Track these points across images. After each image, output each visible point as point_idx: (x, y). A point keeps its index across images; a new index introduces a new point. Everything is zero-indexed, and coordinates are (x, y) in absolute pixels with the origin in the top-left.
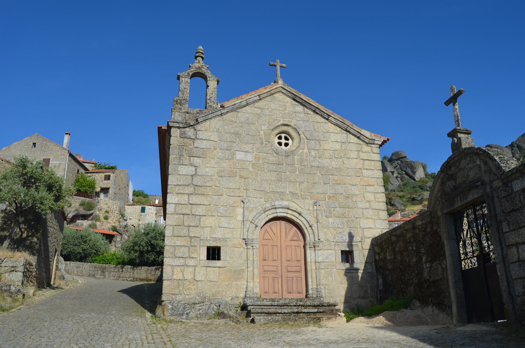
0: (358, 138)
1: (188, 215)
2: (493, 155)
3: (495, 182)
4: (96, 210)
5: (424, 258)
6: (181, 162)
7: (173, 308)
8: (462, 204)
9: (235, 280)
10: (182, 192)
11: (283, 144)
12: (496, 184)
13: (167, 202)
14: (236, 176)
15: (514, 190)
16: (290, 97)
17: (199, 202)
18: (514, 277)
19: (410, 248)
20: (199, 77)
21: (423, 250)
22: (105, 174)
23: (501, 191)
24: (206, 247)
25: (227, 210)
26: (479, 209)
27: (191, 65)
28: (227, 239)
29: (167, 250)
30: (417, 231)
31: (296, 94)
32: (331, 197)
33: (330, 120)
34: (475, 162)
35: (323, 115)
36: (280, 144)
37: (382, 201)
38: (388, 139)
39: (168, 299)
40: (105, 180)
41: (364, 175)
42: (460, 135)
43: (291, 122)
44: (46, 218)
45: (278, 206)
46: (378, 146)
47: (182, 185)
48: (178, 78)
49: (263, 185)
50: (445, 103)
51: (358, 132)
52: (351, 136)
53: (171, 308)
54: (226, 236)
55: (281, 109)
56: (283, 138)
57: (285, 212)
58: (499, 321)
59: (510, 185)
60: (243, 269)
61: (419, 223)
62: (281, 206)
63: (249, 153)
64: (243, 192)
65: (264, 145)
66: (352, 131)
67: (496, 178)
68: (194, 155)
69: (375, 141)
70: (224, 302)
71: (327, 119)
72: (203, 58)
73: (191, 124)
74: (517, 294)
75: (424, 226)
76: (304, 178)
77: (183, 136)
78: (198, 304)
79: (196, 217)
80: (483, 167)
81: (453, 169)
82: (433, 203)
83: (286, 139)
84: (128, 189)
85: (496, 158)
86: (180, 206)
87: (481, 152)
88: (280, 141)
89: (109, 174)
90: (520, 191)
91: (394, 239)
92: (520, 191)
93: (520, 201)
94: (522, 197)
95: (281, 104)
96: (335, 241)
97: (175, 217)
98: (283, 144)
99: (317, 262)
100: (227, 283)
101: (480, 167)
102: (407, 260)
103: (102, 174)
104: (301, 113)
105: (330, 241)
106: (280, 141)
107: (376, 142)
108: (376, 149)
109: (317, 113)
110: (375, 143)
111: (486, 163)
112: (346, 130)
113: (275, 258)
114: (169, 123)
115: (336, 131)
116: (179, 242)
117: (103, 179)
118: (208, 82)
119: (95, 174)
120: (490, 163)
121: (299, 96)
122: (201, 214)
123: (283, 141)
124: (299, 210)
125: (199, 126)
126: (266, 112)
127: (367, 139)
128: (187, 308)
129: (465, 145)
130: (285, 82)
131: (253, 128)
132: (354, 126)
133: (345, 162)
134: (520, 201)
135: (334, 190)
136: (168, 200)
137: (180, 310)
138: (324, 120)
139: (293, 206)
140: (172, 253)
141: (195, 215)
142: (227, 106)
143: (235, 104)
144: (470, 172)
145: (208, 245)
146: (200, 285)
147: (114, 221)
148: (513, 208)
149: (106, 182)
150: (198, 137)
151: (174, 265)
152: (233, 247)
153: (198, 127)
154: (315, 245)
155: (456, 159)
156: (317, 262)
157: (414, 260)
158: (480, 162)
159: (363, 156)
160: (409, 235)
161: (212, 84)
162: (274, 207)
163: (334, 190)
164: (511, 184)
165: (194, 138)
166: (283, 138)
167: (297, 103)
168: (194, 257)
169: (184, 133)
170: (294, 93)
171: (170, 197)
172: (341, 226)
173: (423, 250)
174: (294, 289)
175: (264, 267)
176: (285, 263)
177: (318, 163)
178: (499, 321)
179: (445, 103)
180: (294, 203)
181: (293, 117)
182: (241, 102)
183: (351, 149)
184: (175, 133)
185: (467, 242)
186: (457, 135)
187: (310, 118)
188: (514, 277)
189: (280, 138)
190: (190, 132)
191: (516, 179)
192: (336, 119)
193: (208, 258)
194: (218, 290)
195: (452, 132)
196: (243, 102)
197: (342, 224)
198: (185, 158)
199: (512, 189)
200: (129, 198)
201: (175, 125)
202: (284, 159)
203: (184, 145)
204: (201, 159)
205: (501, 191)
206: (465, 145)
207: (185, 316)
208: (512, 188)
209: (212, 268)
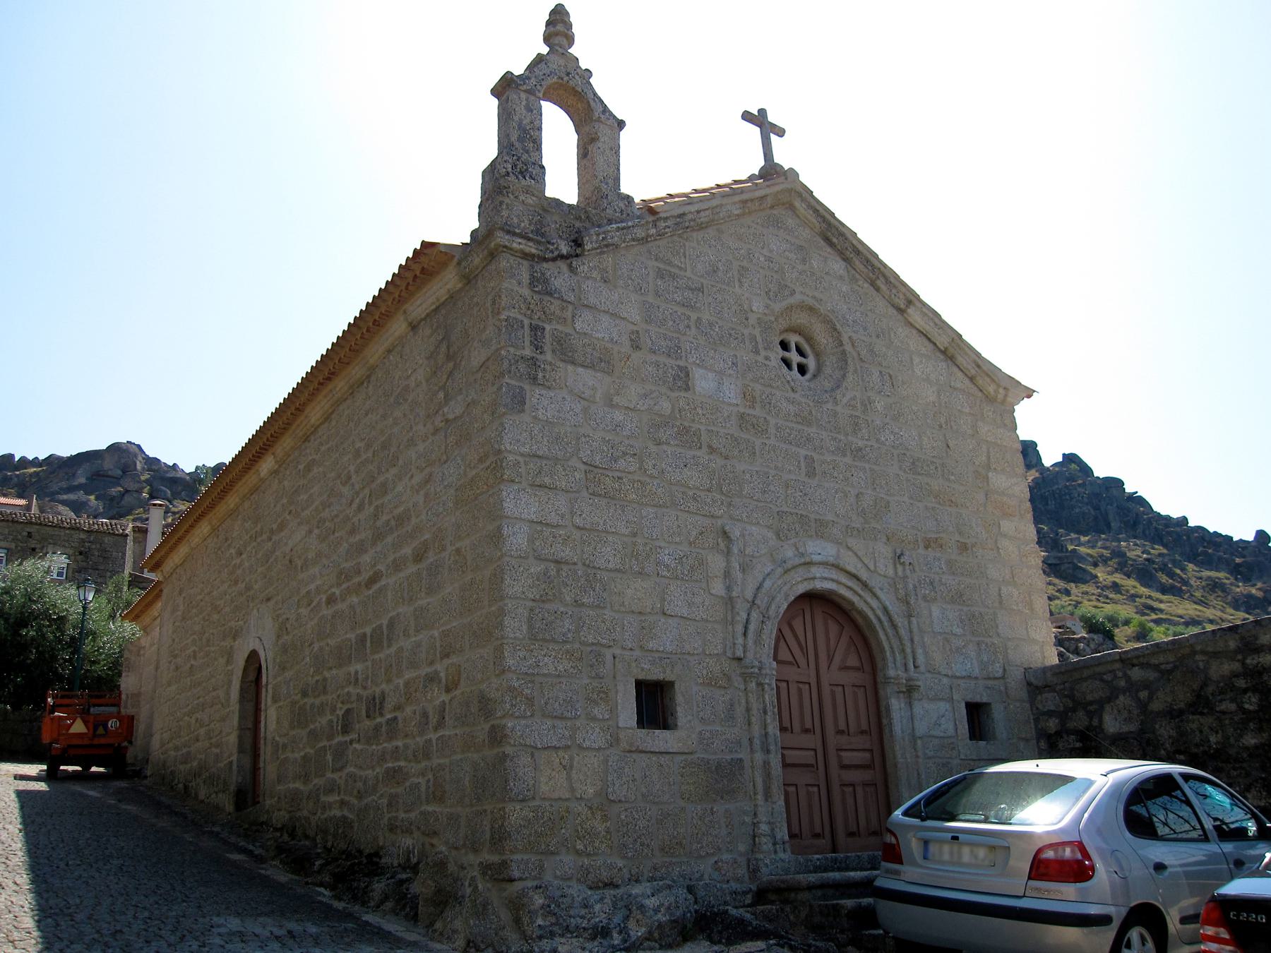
24: (985, 700)
25: (684, 559)
49: (772, 488)
53: (542, 907)
54: (688, 648)
58: (94, 769)
60: (741, 760)
64: (722, 504)
106: (787, 354)
113: (808, 725)
123: (795, 358)
133: (950, 445)
145: (640, 677)
151: (539, 746)
154: (911, 683)
174: (862, 822)
175: (843, 754)
176: (832, 740)
178: (94, 769)
182: (698, 212)
189: (784, 345)
193: (641, 723)
196: (702, 214)
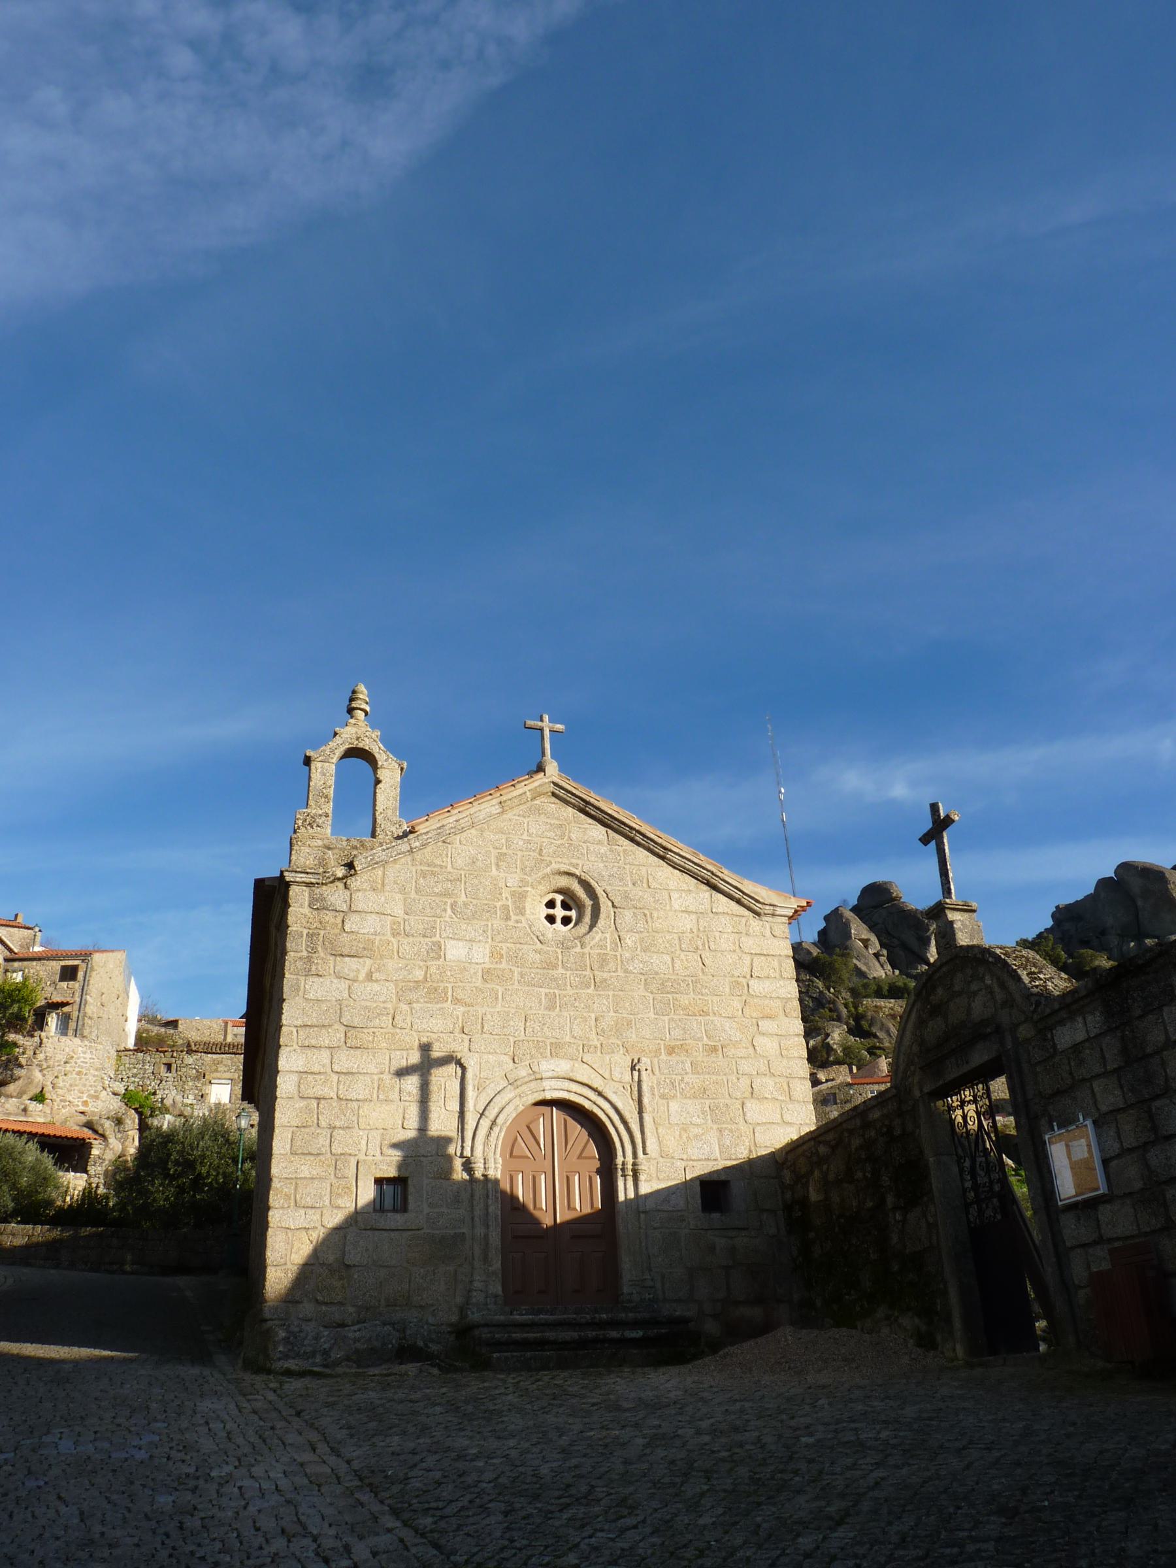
0: (739, 902)
1: (329, 1101)
2: (1015, 967)
3: (1021, 1028)
4: (34, 1067)
5: (890, 1200)
6: (314, 968)
7: (289, 1338)
8: (960, 1073)
9: (443, 1263)
10: (313, 1042)
11: (559, 920)
12: (1025, 1031)
13: (279, 1069)
14: (447, 1001)
15: (1058, 1047)
16: (574, 806)
17: (356, 1066)
18: (1068, 1244)
19: (859, 1175)
20: (357, 757)
21: (885, 1180)
22: (63, 963)
23: (1034, 1048)
26: (971, 1100)
27: (337, 729)
28: (422, 1159)
29: (278, 1189)
30: (873, 1133)
31: (588, 799)
32: (673, 1048)
33: (669, 860)
34: (982, 979)
35: (652, 847)
36: (551, 919)
37: (796, 1055)
38: (808, 903)
39: (276, 1316)
40: (62, 979)
41: (753, 993)
42: (951, 916)
43: (575, 866)
44: (856, 1328)
45: (547, 1073)
46: (785, 920)
47: (316, 1026)
48: (307, 761)
49: (511, 1023)
50: (920, 839)
51: (736, 888)
52: (720, 896)
53: (283, 1339)
55: (551, 834)
56: (558, 904)
57: (563, 1087)
59: (1049, 1036)
61: (876, 1115)
62: (555, 1074)
63: (479, 944)
64: (462, 1041)
65: (511, 923)
66: (722, 886)
67: (1023, 1019)
68: (345, 951)
69: (778, 909)
70: (415, 1320)
71: (663, 858)
72: (366, 713)
73: (338, 876)
74: (1076, 1282)
75: (887, 1122)
76: (609, 1003)
77: (320, 906)
78: (352, 1325)
79: (349, 1105)
80: (1000, 996)
81: (940, 991)
82: (902, 1068)
83: (565, 906)
84: (125, 1005)
85: (1023, 974)
86: (310, 1078)
87: (991, 959)
88: (551, 911)
89: (76, 963)
90: (1070, 1051)
91: (822, 1150)
92: (1070, 1051)
93: (1071, 1074)
94: (1073, 1064)
95: (552, 822)
96: (685, 1157)
97: (297, 1106)
98: (559, 920)
99: (643, 1212)
100: (422, 1270)
101: (992, 993)
102: (854, 1204)
103: (54, 963)
104: (600, 843)
105: (673, 1158)
106: (551, 911)
107: (779, 911)
108: (781, 927)
109: (638, 844)
110: (777, 913)
111: (1002, 985)
112: (708, 884)
114: (286, 874)
115: (685, 887)
116: (306, 1169)
117: (58, 977)
118: (379, 772)
119: (34, 963)
120: (1011, 985)
121: (596, 803)
122: (360, 1097)
123: (559, 912)
124: (597, 1083)
125: (356, 880)
126: (517, 844)
127: (757, 904)
128: (324, 1336)
129: (963, 939)
130: (562, 769)
131: (487, 883)
132: (726, 871)
134: (1071, 1074)
135: (682, 1032)
136: (280, 1063)
137: (306, 1342)
138: (656, 859)
139: (584, 1074)
140: (288, 1197)
141: (347, 1100)
142: (425, 831)
143: (443, 826)
144: (974, 1001)
145: (378, 1176)
146: (356, 1276)
147: (85, 1099)
148: (1058, 1088)
149: (64, 984)
150: (354, 908)
151: (292, 1227)
152: (438, 1178)
153: (353, 883)
155: (944, 969)
156: (643, 1212)
157: (870, 1204)
158: (992, 980)
159: (749, 944)
160: (856, 1142)
161: (390, 774)
162: (538, 1076)
163: (682, 1032)
164: (1052, 1033)
165: (345, 908)
166: (558, 904)
167: (590, 821)
168: (343, 1206)
169: (322, 898)
170: (584, 796)
171: (284, 1056)
172: (698, 1120)
173: (885, 1180)
177: (641, 966)
179: (920, 839)
180: (585, 1066)
181: (582, 854)
182: (457, 821)
183: (721, 929)
184: (299, 899)
185: (979, 1160)
186: (946, 916)
187: (622, 855)
188: (1068, 1244)
190: (336, 896)
191: (1062, 1022)
192: (683, 857)
194: (400, 1288)
195: (935, 909)
197: (701, 1115)
198: (323, 959)
199: (1054, 1046)
200: (126, 1029)
201: (298, 879)
202: (560, 957)
203: (319, 926)
204: (361, 960)
205: (1034, 1048)
206: (963, 939)
207: (318, 1359)
208: (1054, 1044)
209: (385, 1234)
